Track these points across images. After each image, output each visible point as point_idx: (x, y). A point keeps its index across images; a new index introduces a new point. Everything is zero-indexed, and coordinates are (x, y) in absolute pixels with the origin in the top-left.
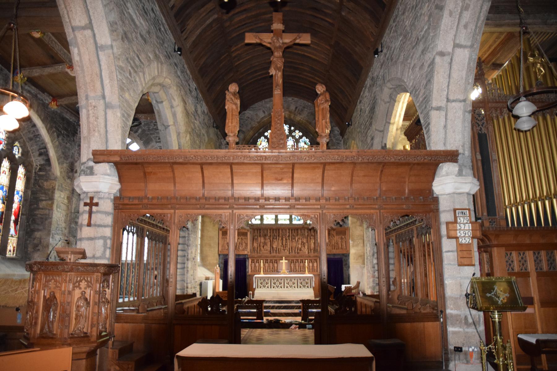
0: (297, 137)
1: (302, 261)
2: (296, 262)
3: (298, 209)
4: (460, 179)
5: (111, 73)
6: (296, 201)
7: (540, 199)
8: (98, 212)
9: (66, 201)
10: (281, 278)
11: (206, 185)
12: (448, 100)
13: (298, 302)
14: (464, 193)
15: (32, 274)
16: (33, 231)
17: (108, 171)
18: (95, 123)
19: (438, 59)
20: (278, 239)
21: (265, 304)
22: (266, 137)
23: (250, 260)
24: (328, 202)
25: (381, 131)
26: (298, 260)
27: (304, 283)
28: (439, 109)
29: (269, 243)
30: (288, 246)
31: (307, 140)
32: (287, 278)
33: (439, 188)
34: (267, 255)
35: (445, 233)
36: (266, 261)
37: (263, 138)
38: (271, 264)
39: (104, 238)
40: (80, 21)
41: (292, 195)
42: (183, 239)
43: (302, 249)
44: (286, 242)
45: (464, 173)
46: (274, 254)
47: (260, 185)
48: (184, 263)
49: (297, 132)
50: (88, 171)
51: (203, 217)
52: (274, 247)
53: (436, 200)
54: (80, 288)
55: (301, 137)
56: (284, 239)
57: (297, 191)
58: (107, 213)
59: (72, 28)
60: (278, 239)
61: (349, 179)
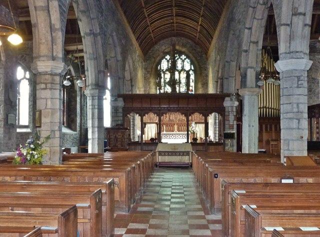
0: (183, 59)
7: (263, 107)
9: (298, 16)
16: (70, 115)
22: (166, 59)
27: (179, 137)
31: (189, 61)
32: (177, 134)
35: (91, 125)
37: (164, 59)
55: (185, 59)
59: (35, 7)
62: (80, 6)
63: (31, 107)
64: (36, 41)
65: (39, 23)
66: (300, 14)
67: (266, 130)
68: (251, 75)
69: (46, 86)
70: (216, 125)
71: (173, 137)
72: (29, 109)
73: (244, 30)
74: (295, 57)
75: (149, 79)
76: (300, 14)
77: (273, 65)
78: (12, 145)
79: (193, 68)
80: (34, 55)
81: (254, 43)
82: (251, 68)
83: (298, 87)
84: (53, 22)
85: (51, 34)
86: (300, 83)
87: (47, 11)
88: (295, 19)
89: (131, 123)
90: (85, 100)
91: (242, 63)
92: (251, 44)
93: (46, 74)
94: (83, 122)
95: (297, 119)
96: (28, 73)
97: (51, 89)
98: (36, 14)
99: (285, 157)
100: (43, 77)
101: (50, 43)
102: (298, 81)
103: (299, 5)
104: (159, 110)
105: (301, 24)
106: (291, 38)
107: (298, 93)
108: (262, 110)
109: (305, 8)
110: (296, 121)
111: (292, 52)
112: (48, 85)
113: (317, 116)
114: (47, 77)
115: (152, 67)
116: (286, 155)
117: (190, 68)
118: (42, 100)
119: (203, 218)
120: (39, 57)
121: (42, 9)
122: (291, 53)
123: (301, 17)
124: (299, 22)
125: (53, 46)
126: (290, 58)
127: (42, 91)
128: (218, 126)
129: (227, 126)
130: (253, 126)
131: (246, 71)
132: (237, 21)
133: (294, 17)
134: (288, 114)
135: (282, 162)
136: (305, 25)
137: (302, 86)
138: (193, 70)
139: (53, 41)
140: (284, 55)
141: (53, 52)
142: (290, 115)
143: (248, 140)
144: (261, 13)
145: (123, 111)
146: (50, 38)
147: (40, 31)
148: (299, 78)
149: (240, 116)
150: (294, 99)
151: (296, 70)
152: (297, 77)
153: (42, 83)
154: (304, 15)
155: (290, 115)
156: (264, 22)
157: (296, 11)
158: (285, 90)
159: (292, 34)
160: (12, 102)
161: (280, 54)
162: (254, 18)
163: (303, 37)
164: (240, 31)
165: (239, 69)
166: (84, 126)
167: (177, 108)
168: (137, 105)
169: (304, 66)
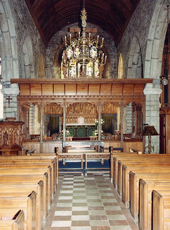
2: (88, 118)
3: (90, 100)
5: (15, 46)
6: (89, 97)
8: (12, 102)
11: (54, 91)
12: (151, 58)
14: (155, 94)
17: (17, 87)
18: (10, 67)
19: (148, 42)
20: (78, 106)
24: (102, 97)
25: (132, 56)
26: (89, 117)
28: (148, 61)
29: (73, 108)
30: (84, 109)
33: (146, 92)
34: (72, 114)
38: (74, 119)
39: (15, 112)
40: (6, 30)
41: (88, 95)
42: (32, 108)
43: (91, 111)
44: (82, 107)
45: (155, 87)
46: (76, 114)
47: (76, 91)
48: (33, 120)
50: (7, 86)
51: (115, 139)
52: (76, 110)
53: (145, 96)
54: (5, 130)
56: (81, 106)
57: (90, 94)
60: (78, 106)
61: (111, 89)
115: (56, 54)
145: (18, 100)
167: (86, 96)
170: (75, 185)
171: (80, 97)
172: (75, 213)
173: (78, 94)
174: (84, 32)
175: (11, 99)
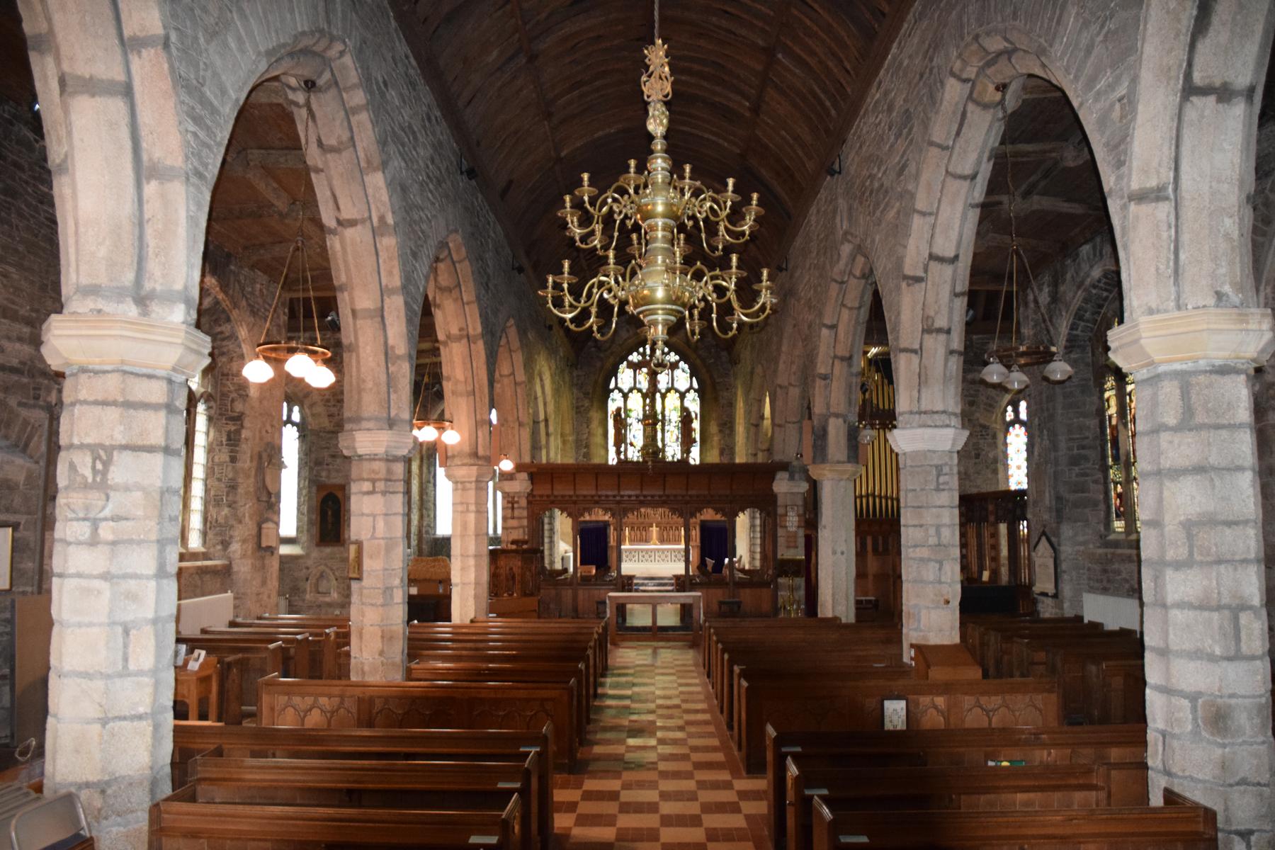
1: (677, 528)
4: (791, 483)
7: (867, 496)
9: (934, 335)
10: (651, 550)
13: (671, 579)
15: (547, 565)
21: (635, 581)
23: (612, 528)
27: (663, 557)
31: (686, 367)
36: (632, 528)
39: (523, 527)
49: (672, 354)
58: (523, 508)
59: (354, 312)
62: (440, 279)
63: (304, 492)
64: (351, 383)
65: (361, 344)
66: (939, 331)
67: (875, 550)
68: (836, 432)
69: (374, 487)
70: (754, 532)
71: (647, 556)
72: (299, 498)
73: (820, 329)
74: (930, 423)
75: (588, 410)
76: (939, 331)
77: (886, 440)
78: (269, 597)
79: (695, 385)
80: (347, 414)
81: (842, 359)
82: (837, 416)
83: (938, 490)
84: (391, 342)
85: (387, 368)
86: (942, 479)
87: (380, 319)
88: (929, 341)
89: (546, 527)
90: (432, 469)
91: (817, 404)
92: (836, 362)
93: (374, 460)
94: (425, 524)
95: (937, 561)
96: (296, 409)
97: (384, 493)
98: (355, 325)
99: (912, 646)
100: (366, 465)
101: (384, 389)
102: (938, 476)
103: (936, 313)
104: (619, 503)
105: (941, 352)
106: (922, 379)
107: (939, 503)
108: (864, 501)
109: (950, 319)
110: (933, 566)
111: (925, 413)
112: (377, 484)
113: (992, 518)
114: (377, 465)
115: (596, 382)
116: (914, 642)
117: (688, 385)
118: (365, 518)
119: (727, 786)
120: (358, 419)
121: (369, 314)
122: (925, 416)
123: (942, 337)
124: (936, 347)
125: (389, 393)
126: (921, 426)
127: (366, 498)
128: (758, 535)
129: (781, 541)
130: (842, 553)
131: (826, 421)
132: (802, 302)
133: (926, 336)
134: (918, 550)
135: (906, 659)
136: (952, 352)
137: (947, 487)
138: (695, 391)
139: (391, 381)
140: (907, 416)
141: (389, 408)
142: (924, 553)
143: (830, 586)
144: (855, 292)
145: (529, 502)
146: (383, 378)
147: (362, 362)
148: (939, 469)
149: (812, 516)
150: (929, 517)
151: (934, 452)
152: (937, 467)
153: (363, 480)
154: (948, 332)
155: (924, 553)
156: (864, 314)
157: (930, 323)
158: (910, 495)
159: (923, 371)
160: (269, 494)
161: (900, 414)
162: (843, 305)
163: (946, 379)
164: (810, 327)
165: (810, 418)
166: (427, 532)
167: (660, 496)
168: (562, 490)
169: (950, 442)
170: (664, 789)
171: (649, 498)
172: (665, 796)
173: (645, 493)
174: (660, 312)
175: (517, 502)
